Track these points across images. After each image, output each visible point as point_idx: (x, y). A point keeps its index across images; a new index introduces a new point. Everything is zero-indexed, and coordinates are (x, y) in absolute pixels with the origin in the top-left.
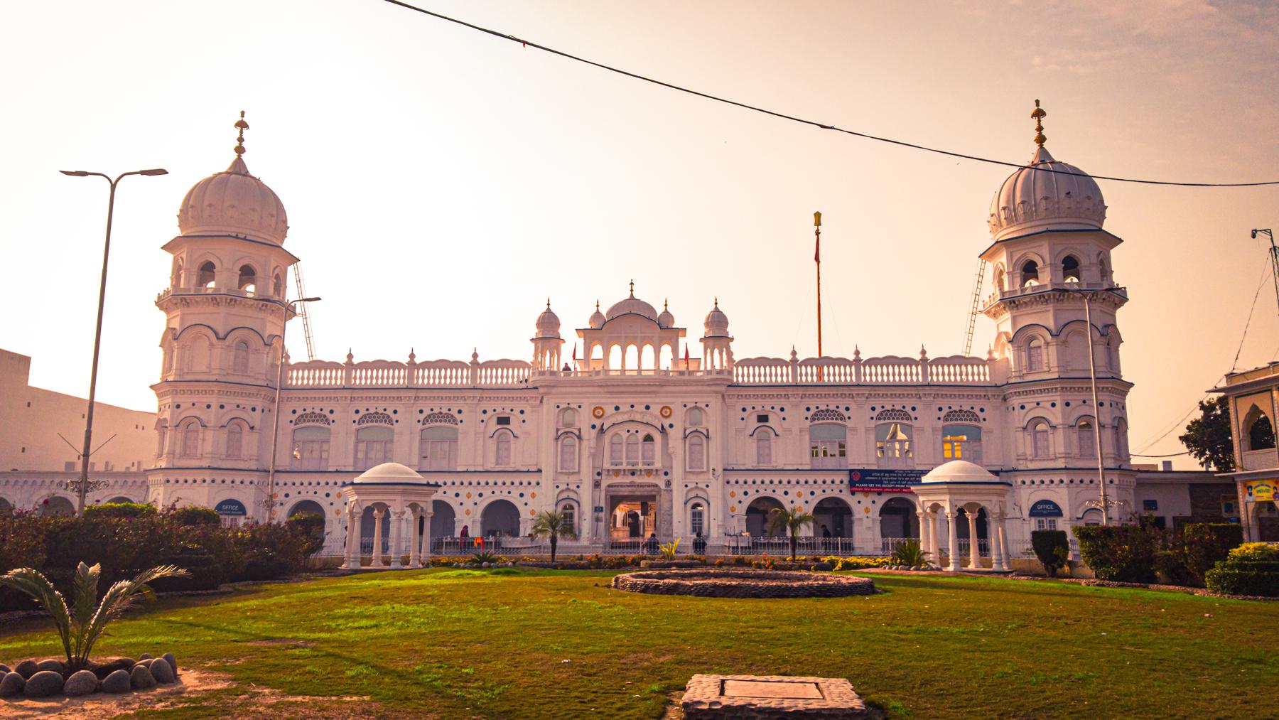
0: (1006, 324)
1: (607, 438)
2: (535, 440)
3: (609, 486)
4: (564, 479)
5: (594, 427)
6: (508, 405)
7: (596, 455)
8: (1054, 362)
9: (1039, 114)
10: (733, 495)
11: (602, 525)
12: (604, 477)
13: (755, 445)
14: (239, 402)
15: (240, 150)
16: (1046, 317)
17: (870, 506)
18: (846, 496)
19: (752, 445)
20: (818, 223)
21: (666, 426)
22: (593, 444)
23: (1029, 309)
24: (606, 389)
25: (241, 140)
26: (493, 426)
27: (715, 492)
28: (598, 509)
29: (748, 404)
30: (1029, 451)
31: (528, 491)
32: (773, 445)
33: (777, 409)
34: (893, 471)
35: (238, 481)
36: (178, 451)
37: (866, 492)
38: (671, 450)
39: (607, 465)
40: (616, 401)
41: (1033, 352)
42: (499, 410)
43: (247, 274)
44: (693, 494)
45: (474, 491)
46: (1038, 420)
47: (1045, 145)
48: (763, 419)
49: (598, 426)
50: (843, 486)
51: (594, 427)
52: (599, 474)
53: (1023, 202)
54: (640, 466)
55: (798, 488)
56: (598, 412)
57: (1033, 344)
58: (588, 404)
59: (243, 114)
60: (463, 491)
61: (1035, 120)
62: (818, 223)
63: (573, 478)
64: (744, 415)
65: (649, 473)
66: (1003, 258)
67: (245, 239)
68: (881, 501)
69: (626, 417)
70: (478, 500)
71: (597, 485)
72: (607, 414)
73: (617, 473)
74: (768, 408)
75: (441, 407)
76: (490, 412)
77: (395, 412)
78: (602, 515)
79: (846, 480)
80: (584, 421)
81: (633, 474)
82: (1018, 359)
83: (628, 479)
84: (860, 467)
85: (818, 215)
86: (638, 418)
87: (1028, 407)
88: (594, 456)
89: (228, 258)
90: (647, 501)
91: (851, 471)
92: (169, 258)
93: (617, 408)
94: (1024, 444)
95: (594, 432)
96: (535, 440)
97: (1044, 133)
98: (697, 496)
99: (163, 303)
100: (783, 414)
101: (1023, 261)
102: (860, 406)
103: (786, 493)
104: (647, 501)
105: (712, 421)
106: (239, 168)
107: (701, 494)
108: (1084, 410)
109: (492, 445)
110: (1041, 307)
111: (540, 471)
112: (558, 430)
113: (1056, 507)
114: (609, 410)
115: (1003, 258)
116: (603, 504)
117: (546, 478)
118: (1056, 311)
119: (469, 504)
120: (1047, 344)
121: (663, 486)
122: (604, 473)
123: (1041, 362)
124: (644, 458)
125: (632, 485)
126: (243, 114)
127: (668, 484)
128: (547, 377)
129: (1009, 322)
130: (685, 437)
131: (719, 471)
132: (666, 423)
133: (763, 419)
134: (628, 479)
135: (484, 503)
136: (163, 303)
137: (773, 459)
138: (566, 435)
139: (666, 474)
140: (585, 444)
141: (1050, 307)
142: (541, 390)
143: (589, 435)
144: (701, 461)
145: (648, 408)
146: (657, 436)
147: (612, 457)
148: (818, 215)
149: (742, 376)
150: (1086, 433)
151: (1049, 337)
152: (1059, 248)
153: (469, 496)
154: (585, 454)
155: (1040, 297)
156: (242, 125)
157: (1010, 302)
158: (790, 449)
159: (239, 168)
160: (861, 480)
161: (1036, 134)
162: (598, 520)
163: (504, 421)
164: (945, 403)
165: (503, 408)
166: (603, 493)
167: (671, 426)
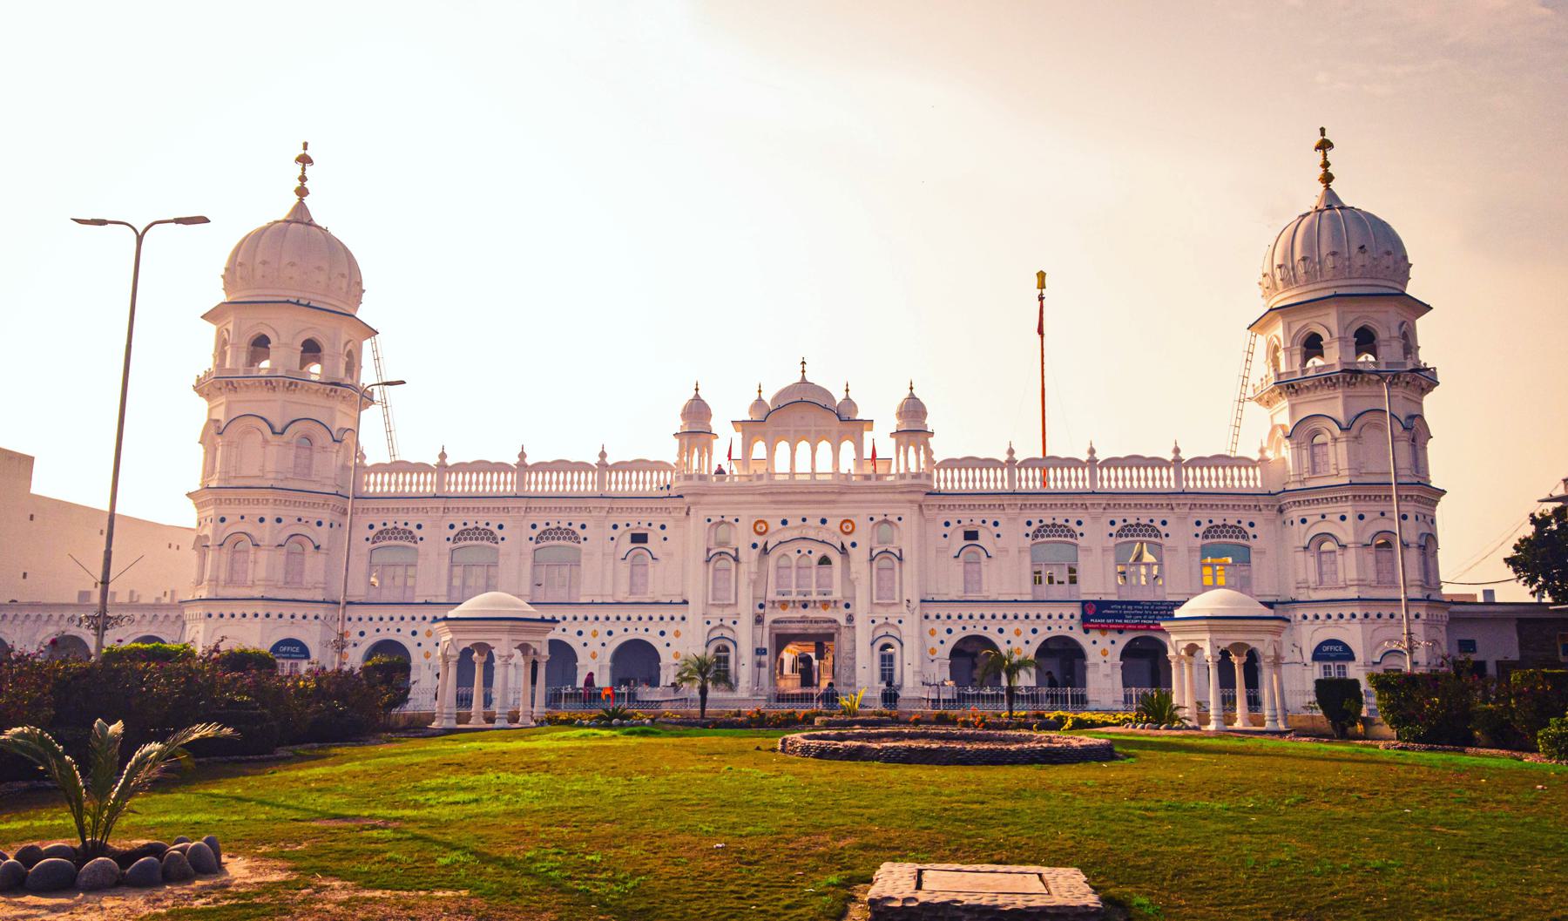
0: (1282, 413)
1: (772, 560)
2: (679, 563)
3: (775, 622)
4: (717, 613)
5: (755, 546)
6: (645, 518)
7: (758, 582)
8: (1343, 464)
9: (1325, 145)
10: (932, 632)
11: (765, 671)
12: (767, 610)
13: (961, 569)
14: (243, 512)
15: (302, 192)
16: (1334, 405)
17: (1109, 647)
18: (1078, 635)
19: (957, 569)
20: (1042, 286)
21: (848, 545)
22: (754, 568)
23: (1311, 396)
24: (770, 498)
25: (303, 179)
26: (626, 545)
27: (910, 630)
28: (760, 651)
29: (952, 516)
30: (1313, 578)
31: (671, 629)
32: (984, 570)
33: (989, 523)
34: (1137, 603)
35: (299, 616)
36: (222, 576)
37: (1103, 629)
38: (853, 576)
39: (771, 596)
40: (784, 513)
41: (1316, 450)
42: (633, 525)
43: (311, 349)
44: (881, 632)
45: (602, 628)
46: (1323, 537)
47: (1333, 185)
48: (971, 535)
49: (761, 546)
50: (1074, 622)
51: (755, 546)
52: (761, 606)
53: (1304, 259)
54: (814, 597)
55: (1017, 625)
56: (760, 527)
57: (1317, 440)
58: (747, 517)
59: (305, 146)
60: (588, 628)
61: (1320, 153)
62: (1042, 286)
63: (728, 612)
64: (947, 530)
65: (825, 604)
66: (1278, 330)
67: (297, 303)
68: (1123, 640)
69: (796, 534)
70: (607, 639)
71: (759, 620)
72: (771, 530)
73: (784, 605)
74: (978, 522)
75: (559, 520)
76: (622, 527)
77: (501, 527)
78: (765, 658)
79: (1078, 614)
80: (742, 538)
81: (805, 606)
82: (1298, 459)
83: (799, 613)
84: (1096, 598)
85: (1041, 276)
86: (811, 534)
87: (1310, 520)
88: (755, 583)
89: (286, 330)
90: (822, 641)
91: (1084, 603)
92: (211, 330)
93: (784, 522)
94: (1306, 567)
95: (756, 552)
96: (679, 563)
97: (1330, 169)
98: (887, 635)
99: (204, 388)
100: (997, 530)
101: (1304, 334)
102: (1095, 519)
103: (1001, 631)
104: (822, 641)
105: (906, 537)
106: (300, 215)
107: (892, 632)
108: (1383, 525)
109: (624, 569)
110: (1326, 393)
111: (685, 602)
112: (708, 550)
113: (1346, 648)
114: (775, 524)
115: (1278, 330)
116: (766, 645)
117: (694, 612)
118: (1346, 398)
119: (595, 645)
120: (1335, 440)
121: (842, 621)
122: (768, 605)
123: (1327, 463)
124: (819, 586)
125: (803, 620)
126: (305, 146)
127: (850, 619)
128: (695, 482)
129: (1286, 412)
130: (872, 560)
131: (915, 601)
132: (848, 541)
133: (971, 535)
134: (799, 613)
135: (614, 643)
136: (204, 388)
137: (985, 587)
138: (719, 556)
139: (847, 606)
140: (743, 567)
141: (1339, 393)
142: (687, 499)
143: (749, 557)
144: (892, 589)
145: (824, 521)
146: (836, 558)
147: (778, 585)
148: (1041, 276)
149: (945, 481)
150: (1384, 554)
151: (1337, 432)
152: (1296, 327)
153: (595, 634)
154: (744, 580)
155: (1326, 381)
156: (305, 160)
157: (1289, 387)
158: (1007, 571)
159: (300, 215)
160: (1097, 614)
161: (1321, 171)
162: (760, 665)
163: (639, 538)
164: (1204, 516)
165: (639, 522)
166: (767, 631)
167: (854, 545)
